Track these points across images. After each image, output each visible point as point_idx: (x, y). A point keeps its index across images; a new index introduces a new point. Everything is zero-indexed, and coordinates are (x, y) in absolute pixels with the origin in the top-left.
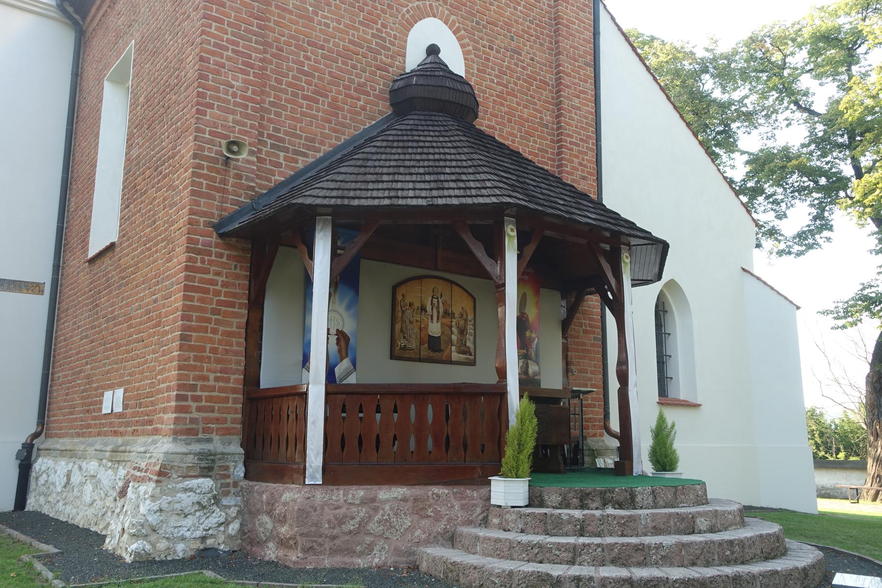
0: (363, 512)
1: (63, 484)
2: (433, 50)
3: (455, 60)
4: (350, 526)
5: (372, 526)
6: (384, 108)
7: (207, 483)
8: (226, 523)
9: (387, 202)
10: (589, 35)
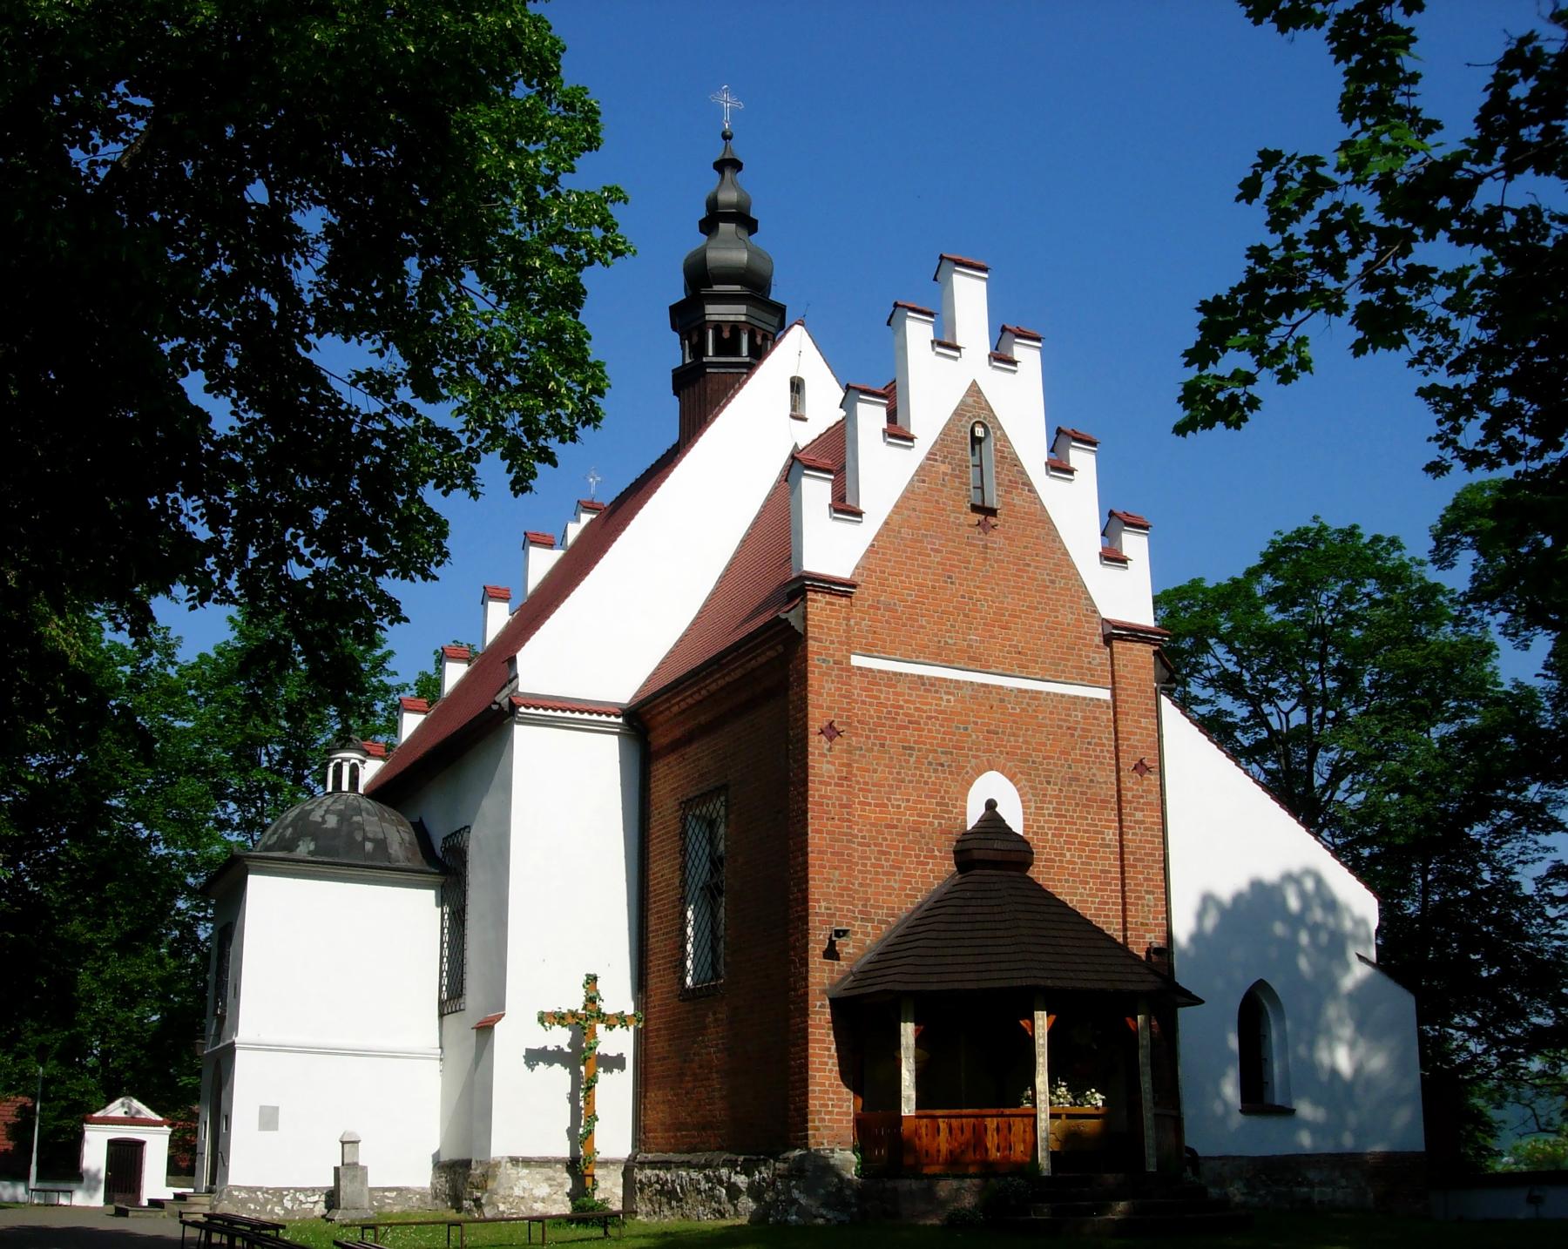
2: (991, 805)
3: (1013, 816)
6: (950, 866)
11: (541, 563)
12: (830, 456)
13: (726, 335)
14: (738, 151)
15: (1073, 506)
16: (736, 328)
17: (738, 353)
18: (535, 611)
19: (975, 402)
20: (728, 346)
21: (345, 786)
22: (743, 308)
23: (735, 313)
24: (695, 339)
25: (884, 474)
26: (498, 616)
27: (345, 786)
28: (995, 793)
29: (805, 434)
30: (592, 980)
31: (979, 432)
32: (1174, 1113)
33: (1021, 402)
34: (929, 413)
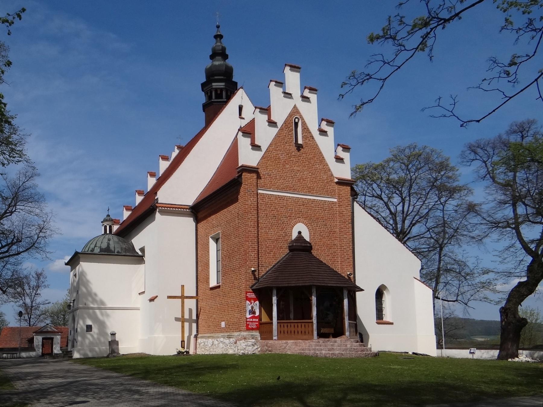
0: (285, 345)
1: (482, 281)
2: (300, 233)
3: (306, 236)
4: (283, 347)
5: (287, 348)
6: (287, 251)
7: (253, 340)
8: (257, 348)
9: (287, 285)
10: (350, 214)
11: (164, 165)
12: (248, 131)
13: (219, 92)
14: (221, 32)
15: (327, 145)
16: (221, 90)
17: (222, 98)
18: (162, 181)
19: (295, 110)
20: (219, 96)
21: (108, 232)
22: (223, 84)
23: (221, 85)
24: (209, 94)
25: (265, 135)
26: (152, 182)
27: (108, 232)
28: (301, 229)
29: (244, 123)
30: (183, 286)
31: (297, 120)
32: (355, 322)
33: (310, 113)
34: (280, 114)
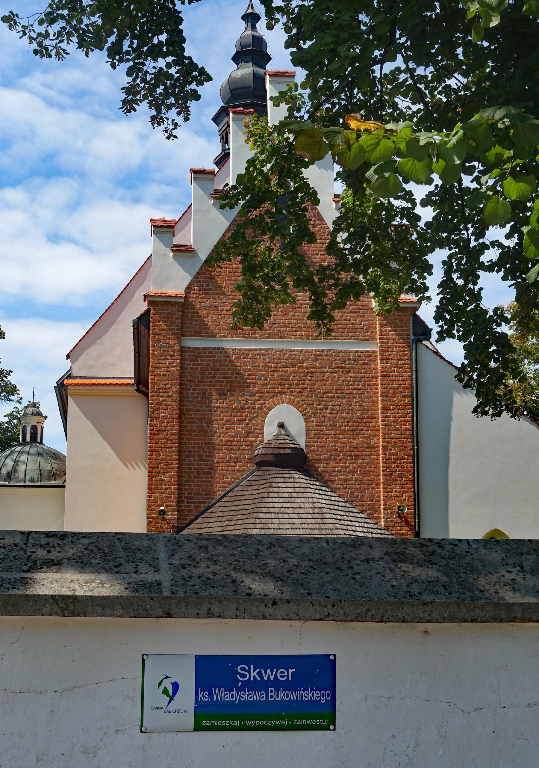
27: (28, 439)
